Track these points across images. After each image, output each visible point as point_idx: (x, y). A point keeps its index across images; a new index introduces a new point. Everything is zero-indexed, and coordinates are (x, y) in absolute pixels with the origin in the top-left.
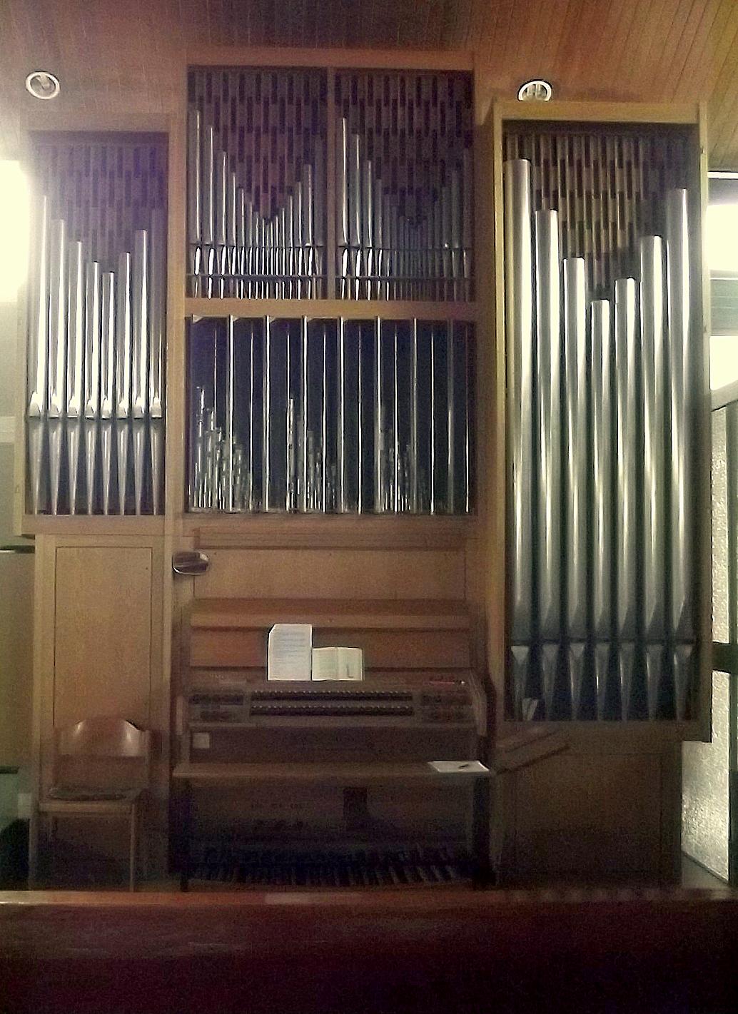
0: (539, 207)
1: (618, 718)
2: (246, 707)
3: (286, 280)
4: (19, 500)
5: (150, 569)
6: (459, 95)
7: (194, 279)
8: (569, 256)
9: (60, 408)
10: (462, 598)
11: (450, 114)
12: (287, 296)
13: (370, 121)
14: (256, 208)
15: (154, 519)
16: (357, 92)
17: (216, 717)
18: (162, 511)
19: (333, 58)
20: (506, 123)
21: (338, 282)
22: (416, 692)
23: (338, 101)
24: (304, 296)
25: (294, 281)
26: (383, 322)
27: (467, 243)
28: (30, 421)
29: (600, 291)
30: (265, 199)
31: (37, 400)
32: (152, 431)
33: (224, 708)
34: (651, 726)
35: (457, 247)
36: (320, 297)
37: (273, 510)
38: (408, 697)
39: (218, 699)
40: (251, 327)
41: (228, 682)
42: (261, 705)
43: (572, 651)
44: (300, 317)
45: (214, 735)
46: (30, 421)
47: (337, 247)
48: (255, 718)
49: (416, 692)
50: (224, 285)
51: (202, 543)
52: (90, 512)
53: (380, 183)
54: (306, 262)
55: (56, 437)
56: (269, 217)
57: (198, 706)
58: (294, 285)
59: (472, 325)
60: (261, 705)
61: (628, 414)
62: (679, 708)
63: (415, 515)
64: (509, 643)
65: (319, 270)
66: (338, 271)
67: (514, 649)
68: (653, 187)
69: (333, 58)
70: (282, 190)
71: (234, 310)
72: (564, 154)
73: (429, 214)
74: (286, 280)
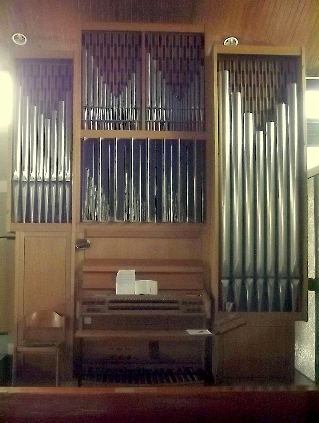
0: (233, 91)
4: (9, 216)
6: (198, 43)
14: (111, 91)
16: (156, 42)
17: (94, 310)
18: (70, 221)
19: (144, 27)
25: (128, 122)
30: (115, 87)
32: (66, 186)
33: (98, 306)
38: (177, 302)
41: (98, 295)
42: (114, 305)
45: (92, 317)
46: (13, 183)
50: (97, 124)
55: (25, 190)
58: (129, 125)
59: (204, 142)
64: (220, 278)
65: (138, 119)
66: (146, 118)
67: (223, 281)
68: (282, 82)
69: (144, 27)
71: (101, 135)
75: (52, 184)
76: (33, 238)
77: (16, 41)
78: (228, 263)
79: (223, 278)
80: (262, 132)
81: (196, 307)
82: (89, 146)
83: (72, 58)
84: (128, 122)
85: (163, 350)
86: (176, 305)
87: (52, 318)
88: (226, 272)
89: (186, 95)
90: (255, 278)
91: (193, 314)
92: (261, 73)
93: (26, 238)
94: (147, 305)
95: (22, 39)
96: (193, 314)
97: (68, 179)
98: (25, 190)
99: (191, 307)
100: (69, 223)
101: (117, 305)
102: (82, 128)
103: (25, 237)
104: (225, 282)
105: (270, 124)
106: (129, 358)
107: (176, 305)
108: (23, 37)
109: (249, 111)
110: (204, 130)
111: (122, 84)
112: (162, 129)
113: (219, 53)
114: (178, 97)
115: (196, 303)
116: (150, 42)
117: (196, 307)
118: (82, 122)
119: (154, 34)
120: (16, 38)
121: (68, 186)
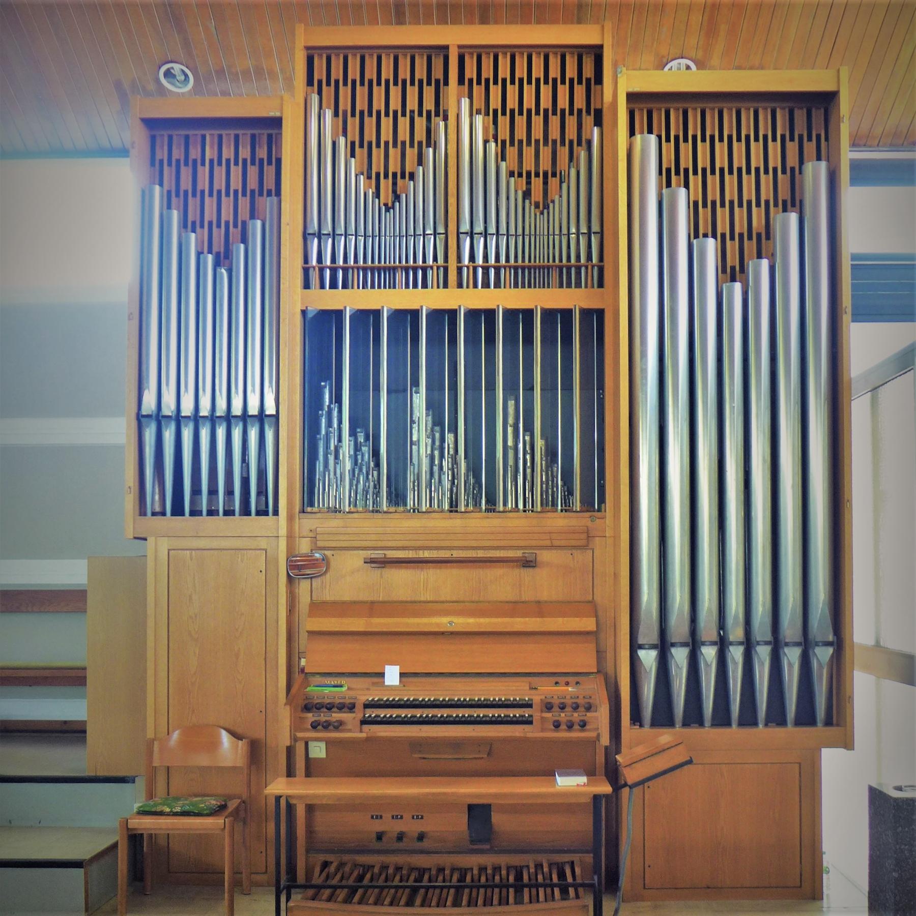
0: (669, 185)
1: (755, 723)
2: (358, 715)
3: (407, 269)
4: (130, 502)
5: (264, 572)
6: (589, 71)
7: (311, 270)
8: (701, 235)
9: (173, 406)
10: (591, 599)
11: (580, 91)
12: (407, 286)
13: (495, 102)
14: (377, 194)
15: (269, 520)
16: (479, 70)
17: (326, 726)
18: (276, 513)
19: (453, 36)
20: (632, 97)
21: (460, 270)
22: (537, 699)
23: (461, 81)
24: (425, 286)
25: (415, 269)
26: (542, 309)
27: (595, 227)
28: (143, 420)
29: (731, 272)
30: (386, 185)
31: (149, 402)
32: (267, 427)
33: (336, 716)
34: (790, 733)
35: (585, 231)
36: (596, 285)
37: (392, 509)
38: (529, 705)
39: (330, 707)
40: (367, 319)
41: (344, 690)
42: (372, 713)
43: (759, 658)
44: (418, 307)
45: (329, 743)
46: (141, 419)
47: (458, 233)
48: (366, 727)
49: (537, 699)
50: (340, 277)
51: (320, 544)
52: (205, 512)
53: (503, 165)
54: (427, 249)
55: (169, 436)
56: (390, 205)
57: (310, 715)
58: (417, 275)
59: (600, 313)
60: (372, 713)
61: (735, 405)
62: (821, 712)
63: (385, 512)
64: (634, 647)
65: (440, 261)
66: (459, 259)
67: (642, 653)
68: (792, 160)
69: (453, 36)
70: (403, 177)
71: (350, 300)
72: (766, 129)
73: (557, 198)
74: (407, 269)
75: (249, 420)
76: (188, 552)
77: (173, 84)
78: (768, 620)
79: (641, 647)
80: (738, 286)
81: (576, 716)
82: (322, 327)
83: (278, 114)
84: (415, 269)
85: (322, 822)
86: (526, 712)
87: (214, 744)
88: (648, 632)
89: (557, 198)
90: (694, 644)
91: (563, 734)
92: (739, 140)
93: (172, 552)
94: (511, 712)
95: (183, 78)
96: (563, 734)
97: (270, 409)
98: (169, 436)
99: (563, 717)
100: (240, 515)
101: (382, 713)
102: (307, 286)
103: (169, 550)
104: (649, 658)
105: (759, 265)
106: (421, 837)
107: (526, 712)
108: (183, 71)
109: (710, 234)
110: (601, 285)
111: (403, 177)
112: (497, 285)
113: (630, 90)
114: (537, 206)
115: (576, 707)
116: (471, 71)
117: (576, 716)
118: (306, 271)
119: (479, 52)
120: (168, 74)
121: (270, 426)
